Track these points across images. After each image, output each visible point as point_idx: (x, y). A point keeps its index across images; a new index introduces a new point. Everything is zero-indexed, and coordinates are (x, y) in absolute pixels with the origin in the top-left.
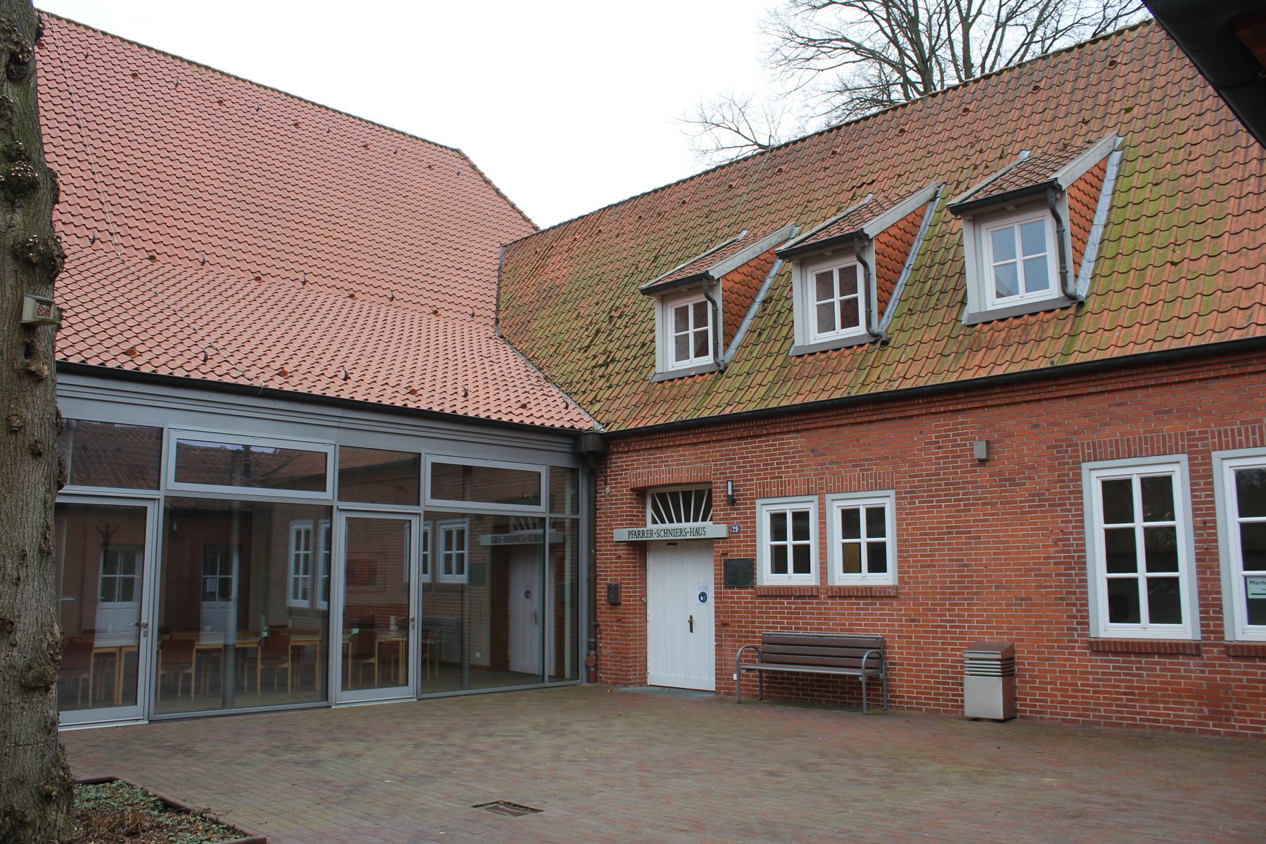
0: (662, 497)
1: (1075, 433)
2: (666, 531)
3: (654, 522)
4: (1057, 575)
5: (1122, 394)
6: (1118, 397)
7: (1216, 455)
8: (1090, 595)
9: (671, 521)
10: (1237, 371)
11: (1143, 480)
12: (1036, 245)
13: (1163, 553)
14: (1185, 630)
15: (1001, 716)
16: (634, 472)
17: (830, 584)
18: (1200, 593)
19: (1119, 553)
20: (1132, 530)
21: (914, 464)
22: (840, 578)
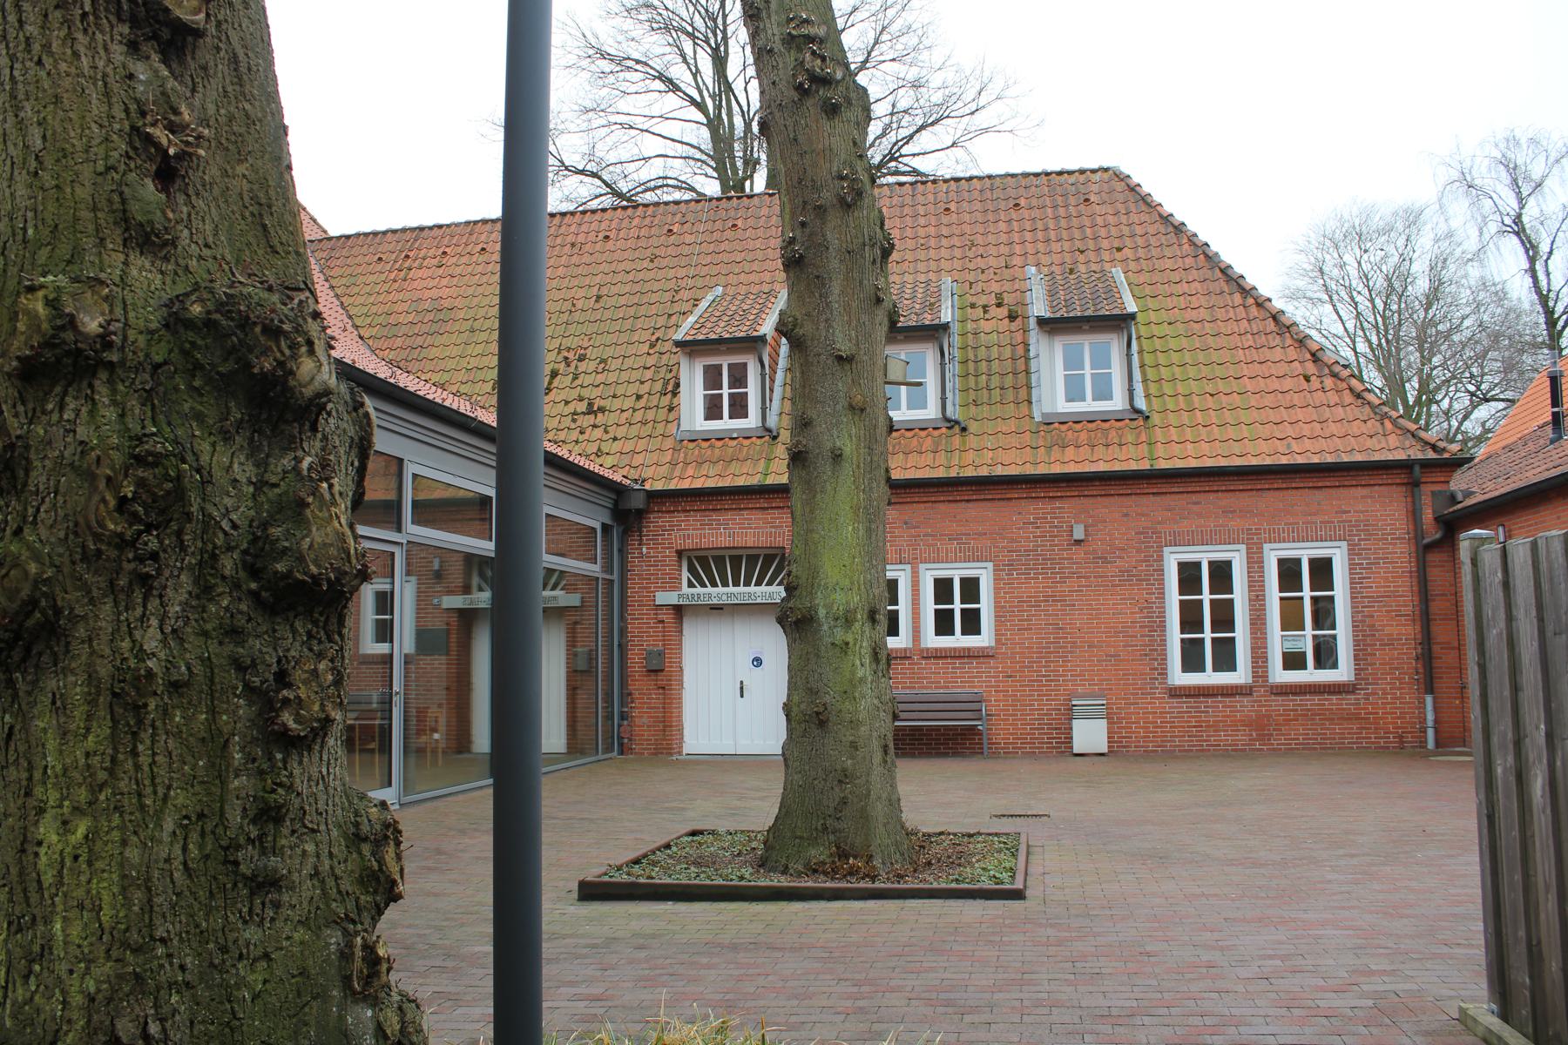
0: (704, 561)
1: (1159, 523)
2: (729, 595)
3: (691, 585)
4: (1142, 636)
5: (1198, 495)
6: (1194, 497)
7: (1266, 546)
8: (1168, 652)
9: (714, 584)
10: (1284, 486)
11: (1210, 563)
12: (1101, 361)
13: (1224, 618)
14: (1240, 676)
15: (1103, 747)
16: (681, 533)
17: (923, 646)
18: (1252, 648)
19: (1190, 618)
20: (1201, 601)
21: (1012, 540)
22: (932, 641)
